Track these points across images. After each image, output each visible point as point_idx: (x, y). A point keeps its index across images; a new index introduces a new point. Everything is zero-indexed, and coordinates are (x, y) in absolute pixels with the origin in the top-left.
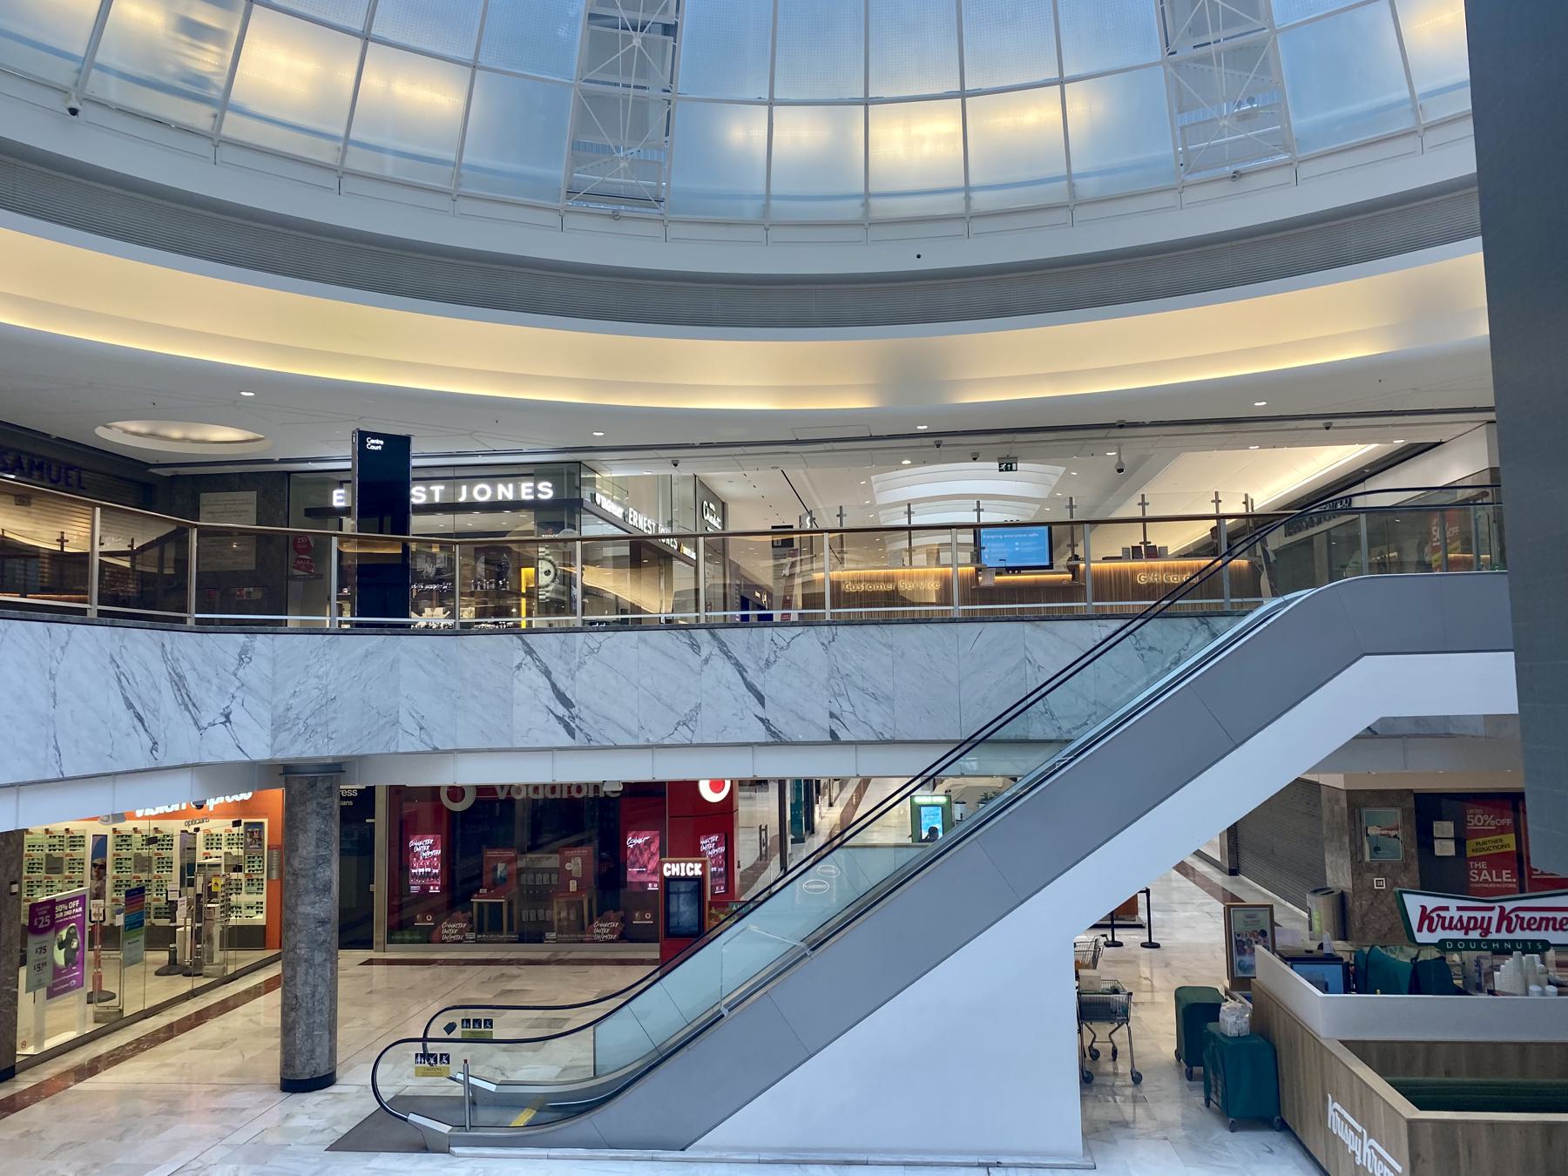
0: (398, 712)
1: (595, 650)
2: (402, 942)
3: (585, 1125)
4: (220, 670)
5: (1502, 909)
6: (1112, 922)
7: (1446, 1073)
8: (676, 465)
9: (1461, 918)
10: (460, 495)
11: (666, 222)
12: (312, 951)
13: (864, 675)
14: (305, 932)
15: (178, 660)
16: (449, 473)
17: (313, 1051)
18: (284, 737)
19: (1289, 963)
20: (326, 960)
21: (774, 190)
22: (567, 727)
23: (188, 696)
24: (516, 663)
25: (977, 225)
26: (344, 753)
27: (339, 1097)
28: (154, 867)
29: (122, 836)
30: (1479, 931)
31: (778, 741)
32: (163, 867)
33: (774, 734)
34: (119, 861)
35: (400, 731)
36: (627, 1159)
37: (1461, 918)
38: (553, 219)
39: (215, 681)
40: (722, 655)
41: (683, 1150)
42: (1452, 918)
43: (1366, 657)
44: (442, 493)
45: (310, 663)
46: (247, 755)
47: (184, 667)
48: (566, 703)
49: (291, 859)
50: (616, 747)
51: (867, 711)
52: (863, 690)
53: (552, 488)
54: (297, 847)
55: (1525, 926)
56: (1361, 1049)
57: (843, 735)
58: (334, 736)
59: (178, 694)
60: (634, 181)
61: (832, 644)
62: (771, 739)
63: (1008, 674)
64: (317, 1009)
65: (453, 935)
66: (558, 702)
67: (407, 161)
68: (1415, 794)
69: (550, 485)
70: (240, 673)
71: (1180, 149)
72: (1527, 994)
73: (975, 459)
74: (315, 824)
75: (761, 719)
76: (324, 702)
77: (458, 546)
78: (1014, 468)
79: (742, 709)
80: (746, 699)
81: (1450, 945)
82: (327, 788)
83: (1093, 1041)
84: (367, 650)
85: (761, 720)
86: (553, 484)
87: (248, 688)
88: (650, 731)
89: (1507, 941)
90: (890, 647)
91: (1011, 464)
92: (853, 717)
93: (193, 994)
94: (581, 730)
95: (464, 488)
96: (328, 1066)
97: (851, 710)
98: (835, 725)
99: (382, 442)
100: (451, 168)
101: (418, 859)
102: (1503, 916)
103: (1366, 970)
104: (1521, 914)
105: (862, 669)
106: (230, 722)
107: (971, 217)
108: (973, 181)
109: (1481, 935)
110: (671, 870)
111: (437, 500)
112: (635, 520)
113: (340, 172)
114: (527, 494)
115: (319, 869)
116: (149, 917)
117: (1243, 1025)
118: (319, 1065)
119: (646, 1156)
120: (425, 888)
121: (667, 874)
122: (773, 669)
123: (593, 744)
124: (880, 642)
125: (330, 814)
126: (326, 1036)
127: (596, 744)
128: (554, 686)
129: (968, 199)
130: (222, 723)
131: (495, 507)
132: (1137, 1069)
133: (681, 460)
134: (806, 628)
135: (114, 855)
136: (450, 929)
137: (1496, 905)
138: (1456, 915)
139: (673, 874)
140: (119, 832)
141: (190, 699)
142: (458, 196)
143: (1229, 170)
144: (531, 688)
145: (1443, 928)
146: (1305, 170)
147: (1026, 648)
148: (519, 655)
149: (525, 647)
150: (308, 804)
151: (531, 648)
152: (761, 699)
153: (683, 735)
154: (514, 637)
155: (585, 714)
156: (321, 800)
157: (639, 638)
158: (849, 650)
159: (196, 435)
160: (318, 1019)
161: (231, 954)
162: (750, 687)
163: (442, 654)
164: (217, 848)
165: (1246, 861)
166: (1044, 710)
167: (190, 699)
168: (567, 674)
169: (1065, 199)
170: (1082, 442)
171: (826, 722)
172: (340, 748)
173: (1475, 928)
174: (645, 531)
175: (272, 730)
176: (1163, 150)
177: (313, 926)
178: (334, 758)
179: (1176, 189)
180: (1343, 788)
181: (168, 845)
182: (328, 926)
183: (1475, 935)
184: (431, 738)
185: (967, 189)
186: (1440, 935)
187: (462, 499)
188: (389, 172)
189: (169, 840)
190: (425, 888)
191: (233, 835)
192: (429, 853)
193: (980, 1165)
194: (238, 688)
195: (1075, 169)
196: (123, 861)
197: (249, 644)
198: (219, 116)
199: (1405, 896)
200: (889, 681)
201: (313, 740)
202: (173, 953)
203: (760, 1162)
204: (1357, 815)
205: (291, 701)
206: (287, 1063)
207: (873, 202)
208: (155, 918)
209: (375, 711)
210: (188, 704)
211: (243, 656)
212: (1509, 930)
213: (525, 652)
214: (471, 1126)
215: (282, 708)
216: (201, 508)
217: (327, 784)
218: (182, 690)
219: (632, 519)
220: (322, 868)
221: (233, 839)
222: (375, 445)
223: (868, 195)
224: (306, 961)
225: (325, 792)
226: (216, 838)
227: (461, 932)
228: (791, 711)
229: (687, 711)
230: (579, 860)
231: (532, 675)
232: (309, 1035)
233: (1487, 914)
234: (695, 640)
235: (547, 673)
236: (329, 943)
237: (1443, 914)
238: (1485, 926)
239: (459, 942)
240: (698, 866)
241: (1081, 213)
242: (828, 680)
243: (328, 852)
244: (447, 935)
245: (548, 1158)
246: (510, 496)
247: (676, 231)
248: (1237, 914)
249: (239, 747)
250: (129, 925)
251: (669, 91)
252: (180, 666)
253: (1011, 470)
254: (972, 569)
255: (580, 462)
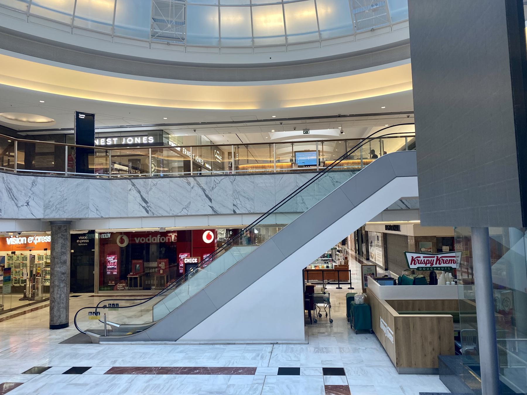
0: (89, 204)
1: (155, 184)
2: (104, 290)
3: (143, 334)
4: (25, 188)
5: (437, 257)
6: (339, 282)
7: (419, 309)
8: (195, 131)
9: (424, 260)
10: (123, 142)
11: (186, 46)
12: (60, 283)
13: (245, 192)
14: (57, 277)
15: (9, 183)
16: (119, 135)
17: (60, 316)
18: (48, 211)
19: (376, 280)
20: (64, 286)
21: (222, 36)
22: (146, 210)
23: (13, 195)
24: (129, 189)
25: (290, 48)
26: (69, 217)
27: (68, 331)
28: (21, 266)
29: (10, 256)
30: (430, 264)
31: (216, 214)
32: (24, 267)
33: (215, 211)
34: (9, 265)
35: (90, 211)
36: (157, 344)
37: (424, 260)
38: (147, 45)
39: (23, 191)
40: (198, 186)
41: (175, 341)
42: (421, 260)
43: (397, 178)
44: (117, 141)
45: (58, 187)
46: (34, 216)
47: (12, 186)
48: (146, 202)
49: (53, 253)
50: (162, 217)
51: (246, 203)
52: (244, 197)
53: (153, 139)
54: (55, 249)
55: (445, 262)
56: (391, 303)
57: (238, 211)
58: (66, 211)
59: (9, 194)
60: (174, 32)
61: (234, 182)
62: (214, 213)
63: (291, 191)
64: (61, 302)
65: (121, 288)
66: (143, 202)
67: (96, 24)
68: (436, 237)
69: (152, 138)
70: (32, 189)
71: (355, 22)
72: (446, 285)
73: (295, 129)
74: (61, 241)
75: (210, 207)
76: (62, 200)
77: (110, 151)
78: (308, 133)
79: (204, 204)
80: (206, 200)
81: (421, 269)
82: (65, 229)
83: (320, 311)
84: (78, 183)
85: (211, 207)
86: (153, 137)
87: (35, 194)
88: (174, 211)
89: (439, 267)
90: (253, 183)
91: (307, 132)
92: (241, 205)
93: (30, 305)
94: (150, 211)
95: (124, 139)
96: (65, 321)
97: (240, 203)
98: (235, 208)
99: (85, 116)
100: (111, 27)
101: (110, 263)
102: (438, 259)
103: (401, 282)
104: (443, 259)
105: (244, 190)
106: (29, 205)
107: (288, 45)
108: (288, 33)
109: (430, 265)
110: (187, 261)
111: (115, 143)
112: (186, 152)
113: (73, 27)
114: (145, 141)
115: (62, 256)
116: (19, 283)
117: (361, 300)
118: (62, 320)
119: (163, 343)
120: (112, 272)
121: (186, 262)
122: (215, 190)
123: (155, 215)
124: (250, 181)
125: (66, 238)
126: (65, 311)
127: (156, 215)
128: (141, 196)
129: (286, 39)
130: (26, 205)
131: (134, 145)
132: (331, 318)
133: (197, 129)
134: (226, 176)
135: (8, 263)
136: (120, 286)
137: (436, 256)
138: (423, 259)
139: (188, 262)
140: (9, 255)
141: (14, 197)
142: (114, 36)
143: (370, 28)
144: (134, 197)
145: (419, 263)
146: (395, 28)
147: (297, 182)
148: (130, 186)
149: (132, 184)
150: (58, 234)
151: (134, 184)
152: (210, 200)
153: (184, 212)
154: (128, 180)
155: (152, 205)
156: (63, 233)
157: (170, 180)
158: (240, 184)
159: (31, 120)
160: (62, 305)
161: (44, 295)
162: (207, 196)
163: (104, 186)
164: (42, 260)
165: (390, 266)
166: (302, 202)
167: (14, 197)
168: (146, 192)
169: (318, 38)
170: (329, 123)
171: (232, 208)
172: (68, 215)
173: (429, 263)
174: (201, 163)
175: (44, 208)
176: (349, 22)
177: (60, 275)
178: (67, 219)
179: (354, 35)
180: (413, 236)
181: (25, 259)
182: (66, 275)
183: (429, 265)
184: (100, 213)
185: (286, 36)
186: (418, 265)
187: (123, 143)
188: (90, 27)
189: (26, 258)
190: (112, 272)
191: (48, 256)
192: (113, 261)
193: (271, 344)
194: (32, 194)
195: (321, 29)
196: (11, 265)
197: (36, 180)
198: (28, 7)
199: (407, 253)
200: (253, 194)
201: (59, 212)
202: (25, 294)
203: (200, 344)
204: (418, 245)
205: (50, 199)
206: (51, 320)
207: (255, 40)
208: (21, 283)
209: (81, 204)
210: (13, 198)
211: (34, 184)
212: (439, 264)
213: (132, 185)
214: (106, 335)
215: (47, 201)
216: (36, 146)
217: (65, 228)
218: (11, 193)
219: (184, 152)
220: (63, 256)
221: (47, 257)
222: (82, 116)
223: (253, 38)
224: (57, 286)
225: (64, 231)
226: (42, 257)
227: (123, 286)
228: (220, 204)
229: (186, 204)
230: (164, 263)
231: (134, 193)
232: (59, 310)
233: (432, 259)
234: (188, 181)
235: (139, 192)
236: (66, 280)
237: (418, 259)
238: (432, 263)
239: (123, 290)
240: (196, 259)
241: (323, 43)
242: (233, 194)
243: (65, 251)
244: (119, 288)
245: (131, 344)
246: (139, 142)
247: (189, 49)
248: (365, 268)
249: (32, 214)
250: (5, 280)
251: (184, 1)
252: (10, 185)
253: (307, 133)
254: (291, 163)
255: (163, 130)
